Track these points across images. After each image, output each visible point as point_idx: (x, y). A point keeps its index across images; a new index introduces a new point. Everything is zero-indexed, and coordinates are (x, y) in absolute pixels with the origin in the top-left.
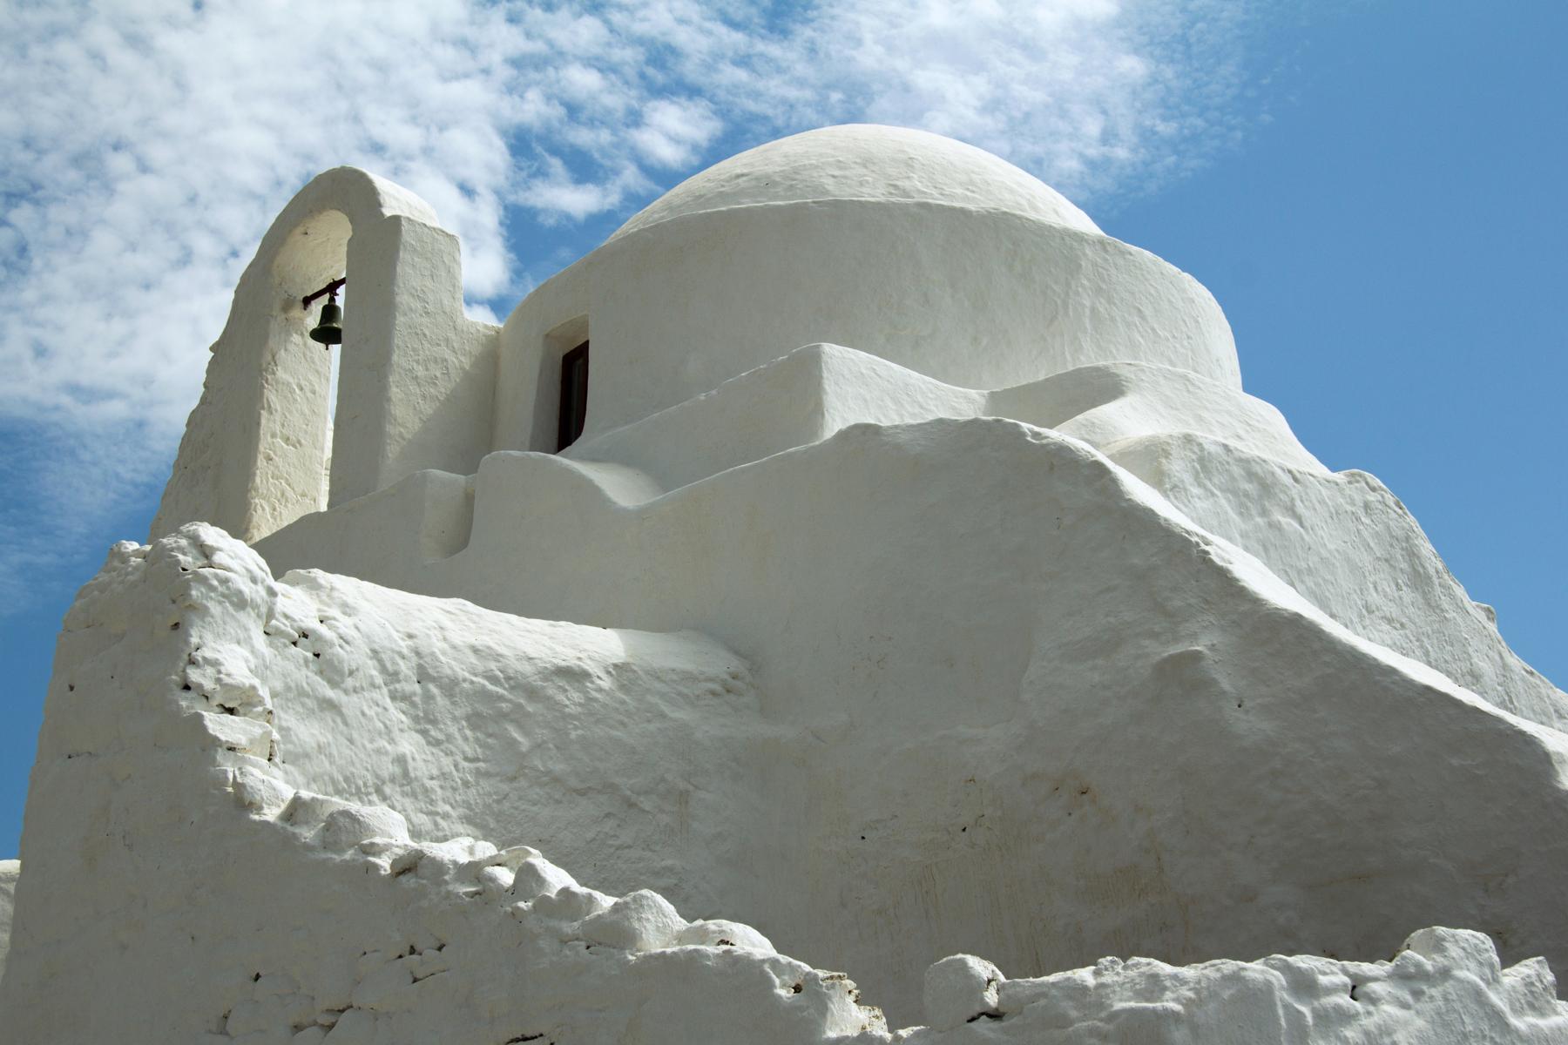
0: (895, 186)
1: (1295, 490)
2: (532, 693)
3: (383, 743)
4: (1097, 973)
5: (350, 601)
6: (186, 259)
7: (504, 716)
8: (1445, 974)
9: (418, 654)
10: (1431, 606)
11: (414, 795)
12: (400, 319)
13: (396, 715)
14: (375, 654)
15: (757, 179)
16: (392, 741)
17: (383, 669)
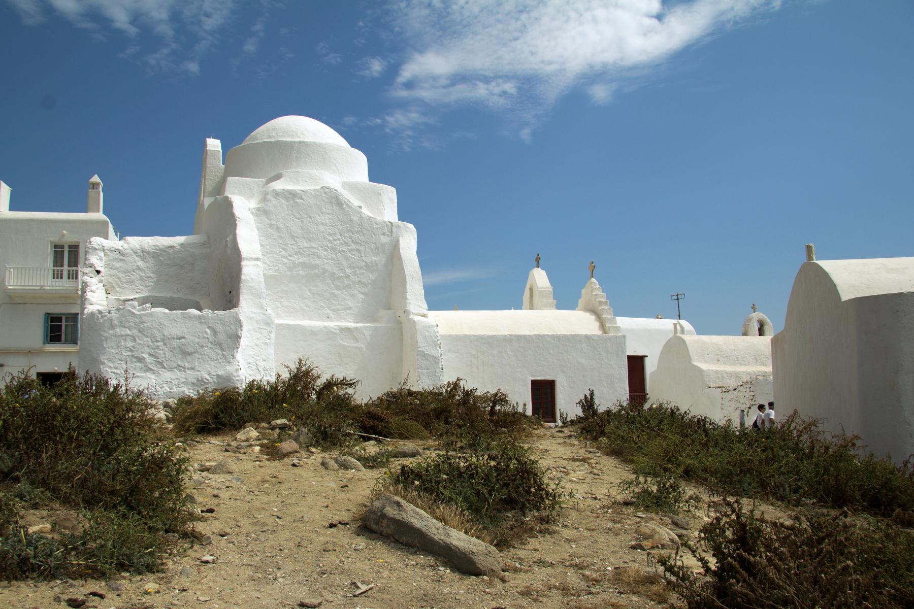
2: (164, 251)
6: (568, 19)
7: (159, 256)
12: (208, 170)
14: (132, 250)
17: (134, 252)
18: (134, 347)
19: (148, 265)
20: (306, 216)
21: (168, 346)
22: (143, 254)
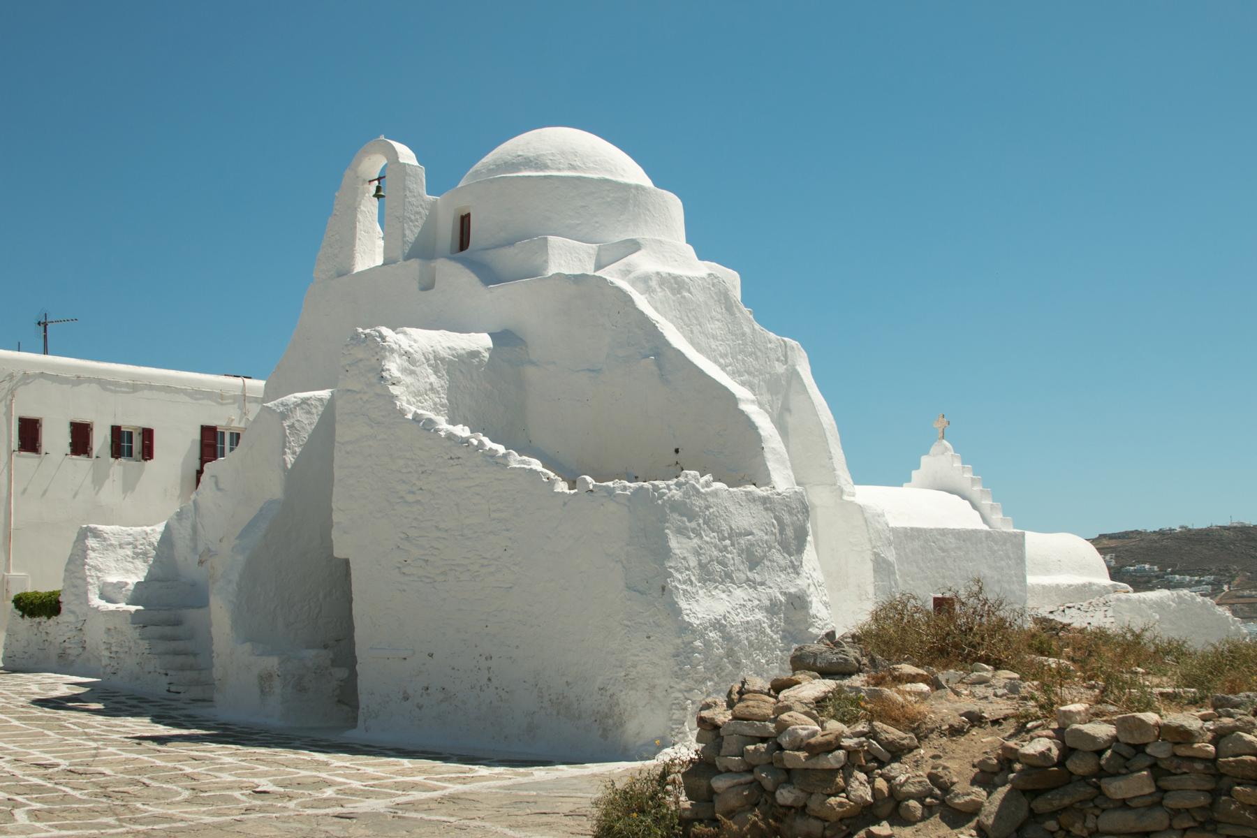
0: (571, 164)
1: (691, 283)
3: (426, 380)
4: (613, 484)
5: (416, 338)
8: (687, 482)
9: (434, 352)
10: (732, 313)
11: (434, 393)
13: (430, 371)
15: (525, 159)
16: (429, 379)
17: (426, 358)
18: (701, 548)
19: (443, 382)
20: (695, 322)
21: (736, 546)
22: (437, 362)
